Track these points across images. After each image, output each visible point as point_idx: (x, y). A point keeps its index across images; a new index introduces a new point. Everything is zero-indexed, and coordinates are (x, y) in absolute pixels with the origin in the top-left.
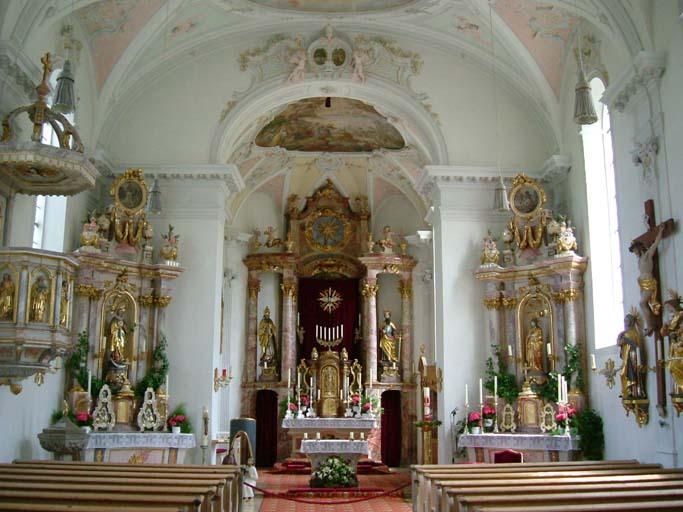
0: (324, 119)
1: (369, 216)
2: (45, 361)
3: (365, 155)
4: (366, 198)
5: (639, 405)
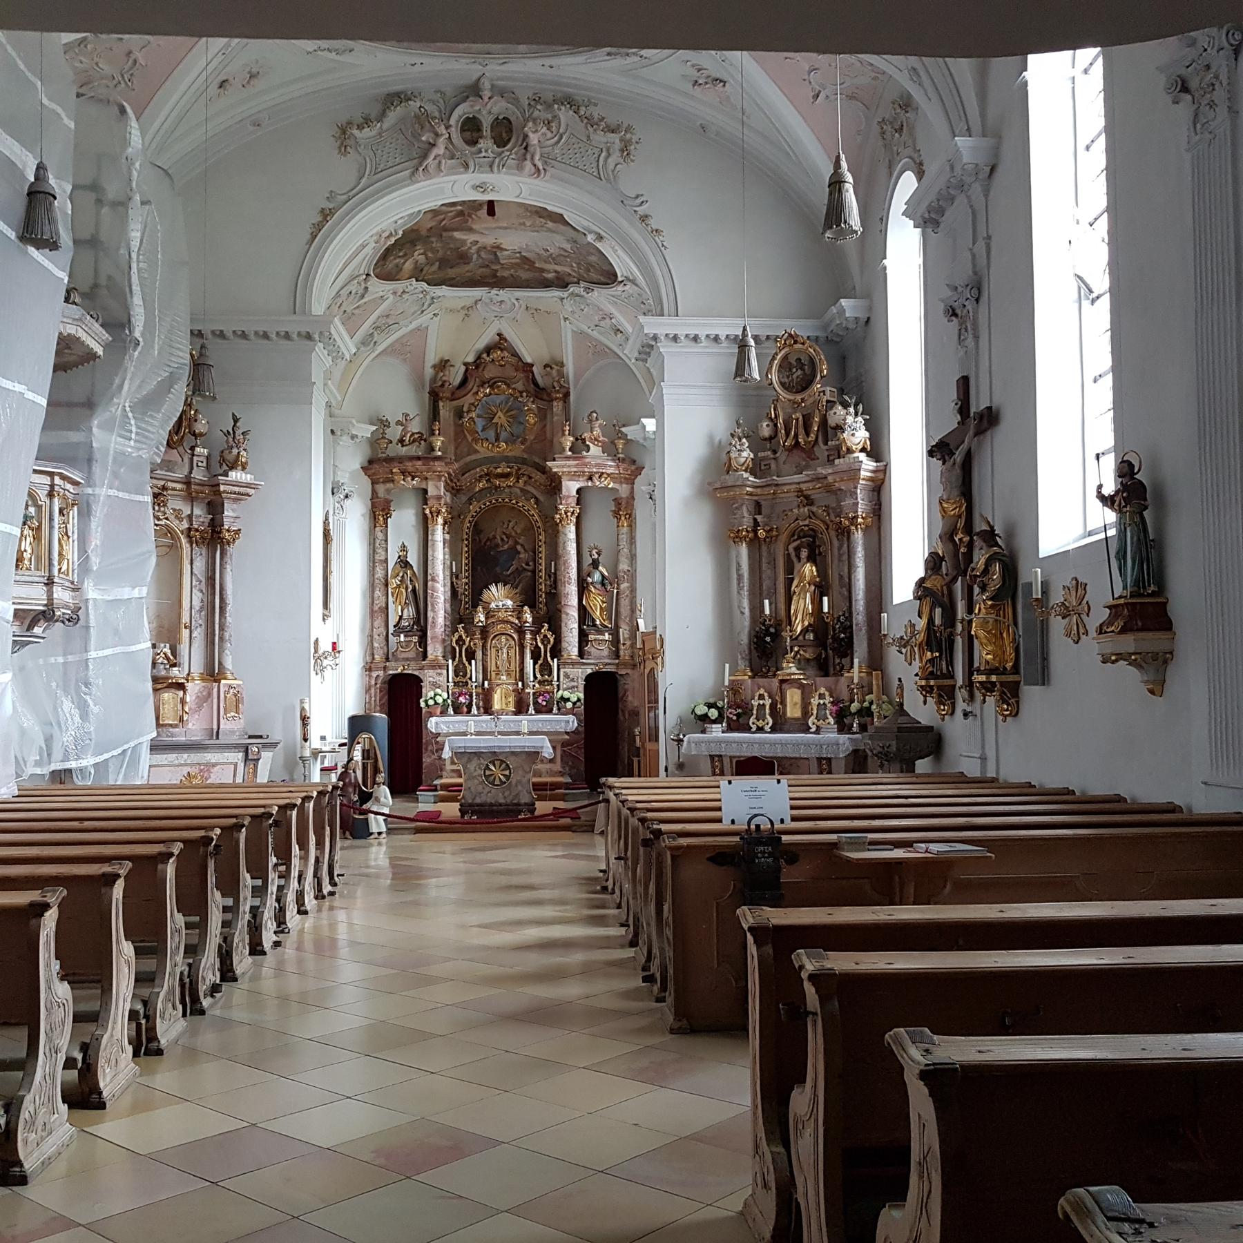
0: (483, 234)
1: (567, 395)
2: (37, 630)
3: (556, 293)
4: (562, 365)
5: (939, 688)
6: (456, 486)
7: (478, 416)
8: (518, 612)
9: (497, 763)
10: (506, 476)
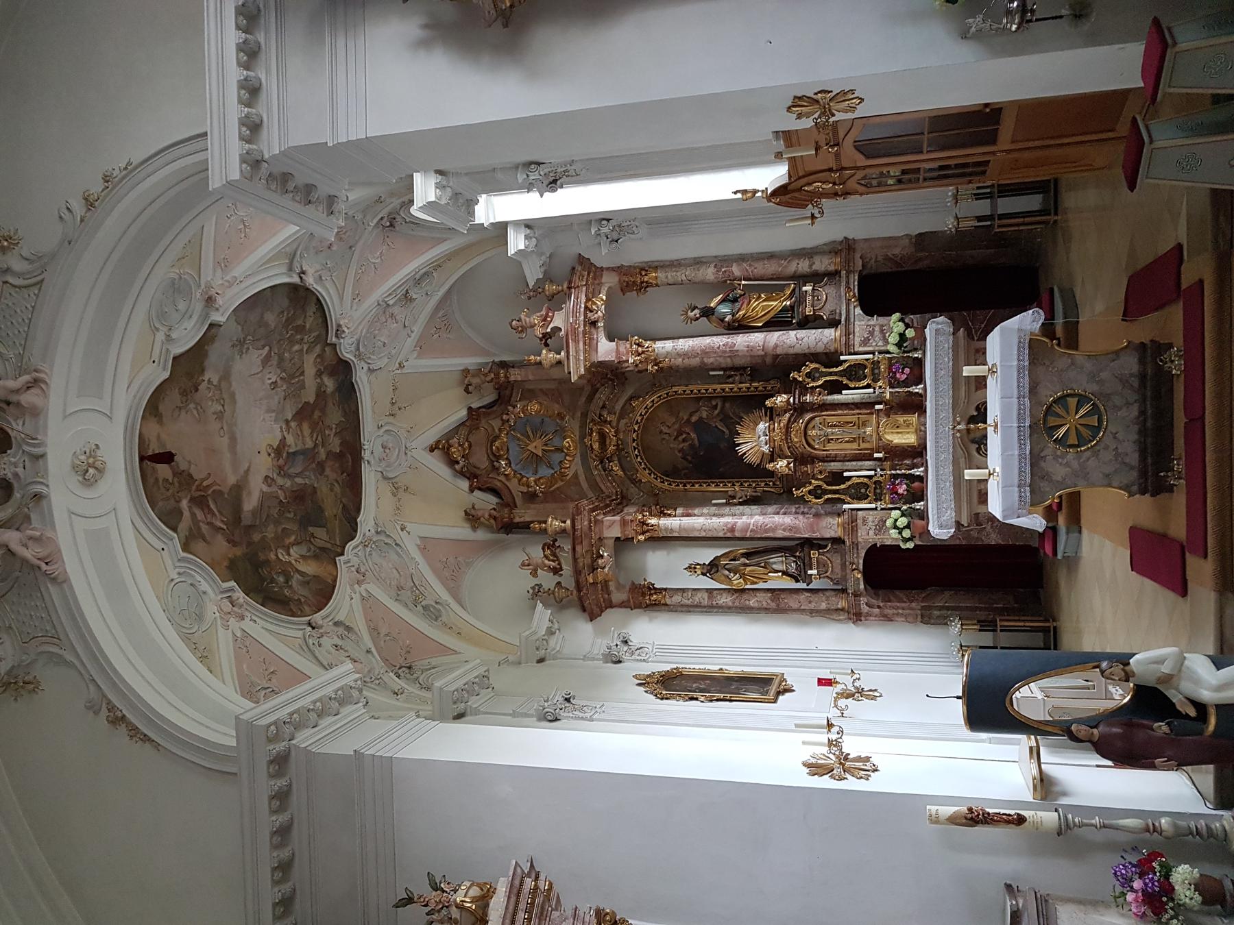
1: (504, 365)
3: (361, 378)
4: (466, 372)
6: (616, 499)
7: (536, 472)
8: (772, 414)
9: (1052, 421)
10: (603, 437)
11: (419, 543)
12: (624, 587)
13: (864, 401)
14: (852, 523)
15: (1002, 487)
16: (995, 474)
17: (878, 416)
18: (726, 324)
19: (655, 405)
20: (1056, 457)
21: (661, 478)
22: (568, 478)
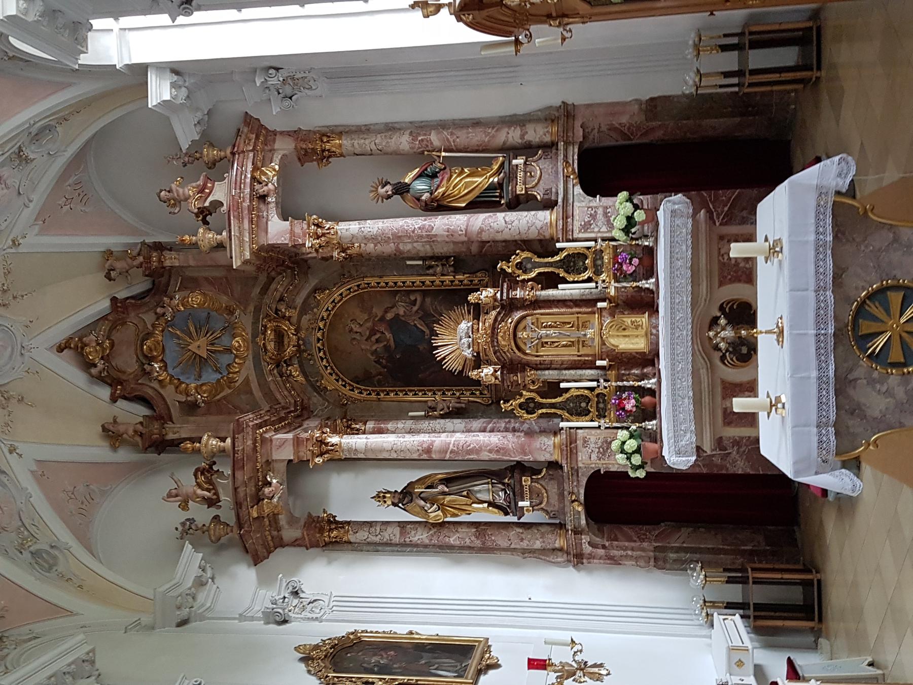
1: (159, 247)
4: (108, 254)
6: (296, 410)
8: (477, 311)
9: (866, 327)
10: (280, 337)
11: (34, 468)
12: (297, 520)
13: (584, 297)
14: (571, 444)
15: (793, 427)
16: (780, 405)
17: (601, 316)
18: (423, 204)
19: (344, 299)
20: (871, 382)
21: (350, 385)
22: (237, 384)
